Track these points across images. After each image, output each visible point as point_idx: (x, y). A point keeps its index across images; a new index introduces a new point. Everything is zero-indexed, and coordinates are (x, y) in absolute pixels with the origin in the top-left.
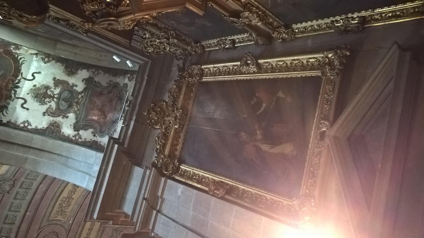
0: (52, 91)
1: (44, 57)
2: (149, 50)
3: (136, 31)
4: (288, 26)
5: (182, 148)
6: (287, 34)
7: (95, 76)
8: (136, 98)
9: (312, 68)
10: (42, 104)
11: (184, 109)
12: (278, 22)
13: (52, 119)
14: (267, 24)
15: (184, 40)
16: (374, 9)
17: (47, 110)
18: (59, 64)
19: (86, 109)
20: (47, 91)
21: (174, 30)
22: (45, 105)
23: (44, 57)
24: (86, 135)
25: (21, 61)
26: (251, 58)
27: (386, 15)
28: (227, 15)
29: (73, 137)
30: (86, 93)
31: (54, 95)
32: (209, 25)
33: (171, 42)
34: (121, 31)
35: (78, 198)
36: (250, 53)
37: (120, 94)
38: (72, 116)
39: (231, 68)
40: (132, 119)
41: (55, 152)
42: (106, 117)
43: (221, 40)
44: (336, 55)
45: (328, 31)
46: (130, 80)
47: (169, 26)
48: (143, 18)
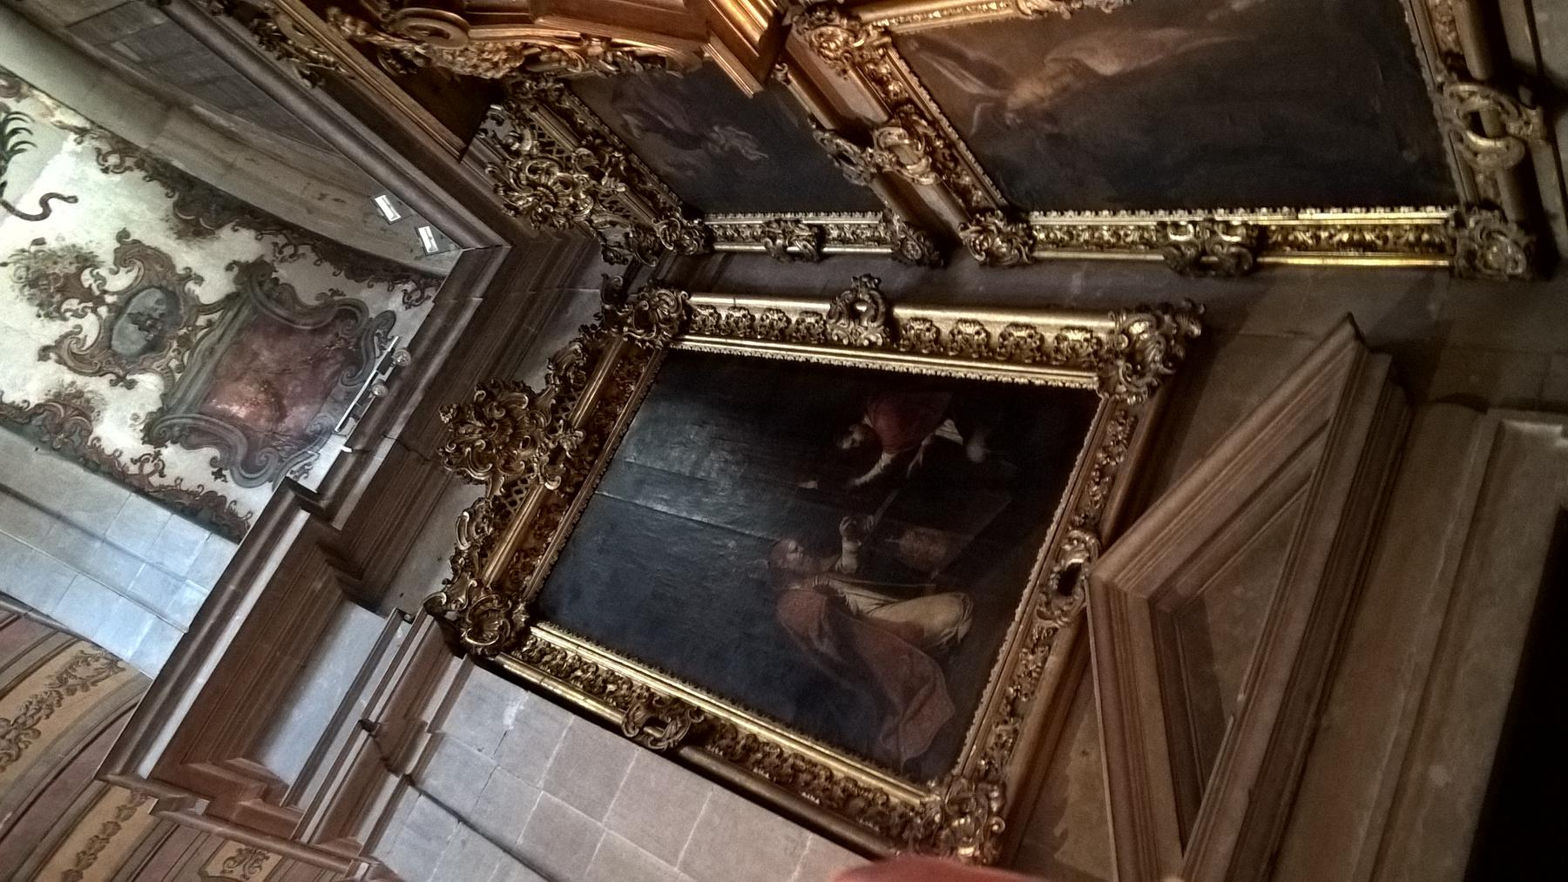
0: (98, 277)
1: (105, 148)
2: (520, 199)
3: (493, 118)
4: (1015, 214)
5: (553, 567)
6: (1008, 239)
7: (282, 260)
8: (421, 363)
9: (1072, 361)
10: (48, 315)
11: (596, 428)
12: (987, 191)
13: (69, 377)
14: (949, 188)
15: (651, 196)
16: (1298, 206)
17: (59, 343)
18: (155, 187)
19: (214, 371)
20: (81, 270)
21: (627, 151)
22: (59, 322)
23: (105, 148)
24: (187, 466)
25: (13, 140)
26: (871, 297)
27: (1331, 236)
28: (827, 124)
29: (134, 461)
30: (231, 314)
31: (105, 292)
32: (754, 155)
33: (604, 191)
34: (462, 77)
35: (60, 737)
36: (871, 278)
37: (357, 345)
38: (150, 385)
39: (794, 320)
40: (385, 435)
41: (44, 502)
42: (281, 413)
43: (778, 221)
44: (1158, 327)
45: (1141, 257)
46: (408, 303)
47: (612, 132)
48: (554, 49)
